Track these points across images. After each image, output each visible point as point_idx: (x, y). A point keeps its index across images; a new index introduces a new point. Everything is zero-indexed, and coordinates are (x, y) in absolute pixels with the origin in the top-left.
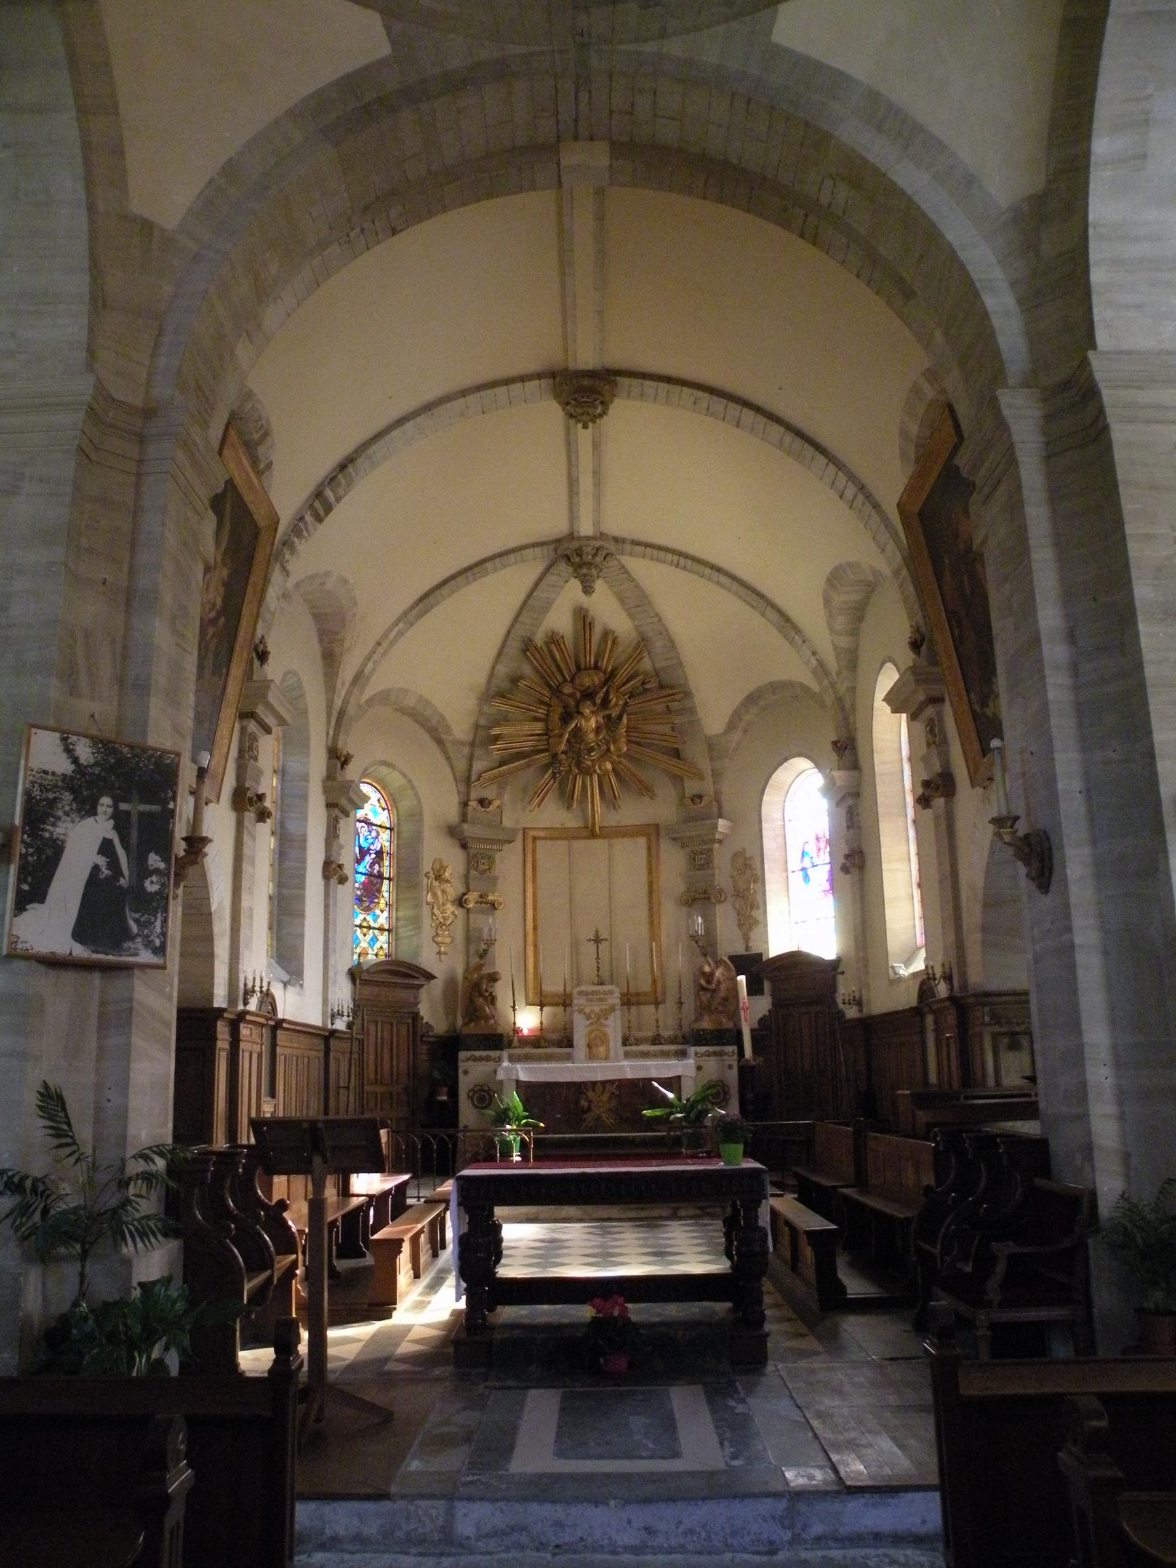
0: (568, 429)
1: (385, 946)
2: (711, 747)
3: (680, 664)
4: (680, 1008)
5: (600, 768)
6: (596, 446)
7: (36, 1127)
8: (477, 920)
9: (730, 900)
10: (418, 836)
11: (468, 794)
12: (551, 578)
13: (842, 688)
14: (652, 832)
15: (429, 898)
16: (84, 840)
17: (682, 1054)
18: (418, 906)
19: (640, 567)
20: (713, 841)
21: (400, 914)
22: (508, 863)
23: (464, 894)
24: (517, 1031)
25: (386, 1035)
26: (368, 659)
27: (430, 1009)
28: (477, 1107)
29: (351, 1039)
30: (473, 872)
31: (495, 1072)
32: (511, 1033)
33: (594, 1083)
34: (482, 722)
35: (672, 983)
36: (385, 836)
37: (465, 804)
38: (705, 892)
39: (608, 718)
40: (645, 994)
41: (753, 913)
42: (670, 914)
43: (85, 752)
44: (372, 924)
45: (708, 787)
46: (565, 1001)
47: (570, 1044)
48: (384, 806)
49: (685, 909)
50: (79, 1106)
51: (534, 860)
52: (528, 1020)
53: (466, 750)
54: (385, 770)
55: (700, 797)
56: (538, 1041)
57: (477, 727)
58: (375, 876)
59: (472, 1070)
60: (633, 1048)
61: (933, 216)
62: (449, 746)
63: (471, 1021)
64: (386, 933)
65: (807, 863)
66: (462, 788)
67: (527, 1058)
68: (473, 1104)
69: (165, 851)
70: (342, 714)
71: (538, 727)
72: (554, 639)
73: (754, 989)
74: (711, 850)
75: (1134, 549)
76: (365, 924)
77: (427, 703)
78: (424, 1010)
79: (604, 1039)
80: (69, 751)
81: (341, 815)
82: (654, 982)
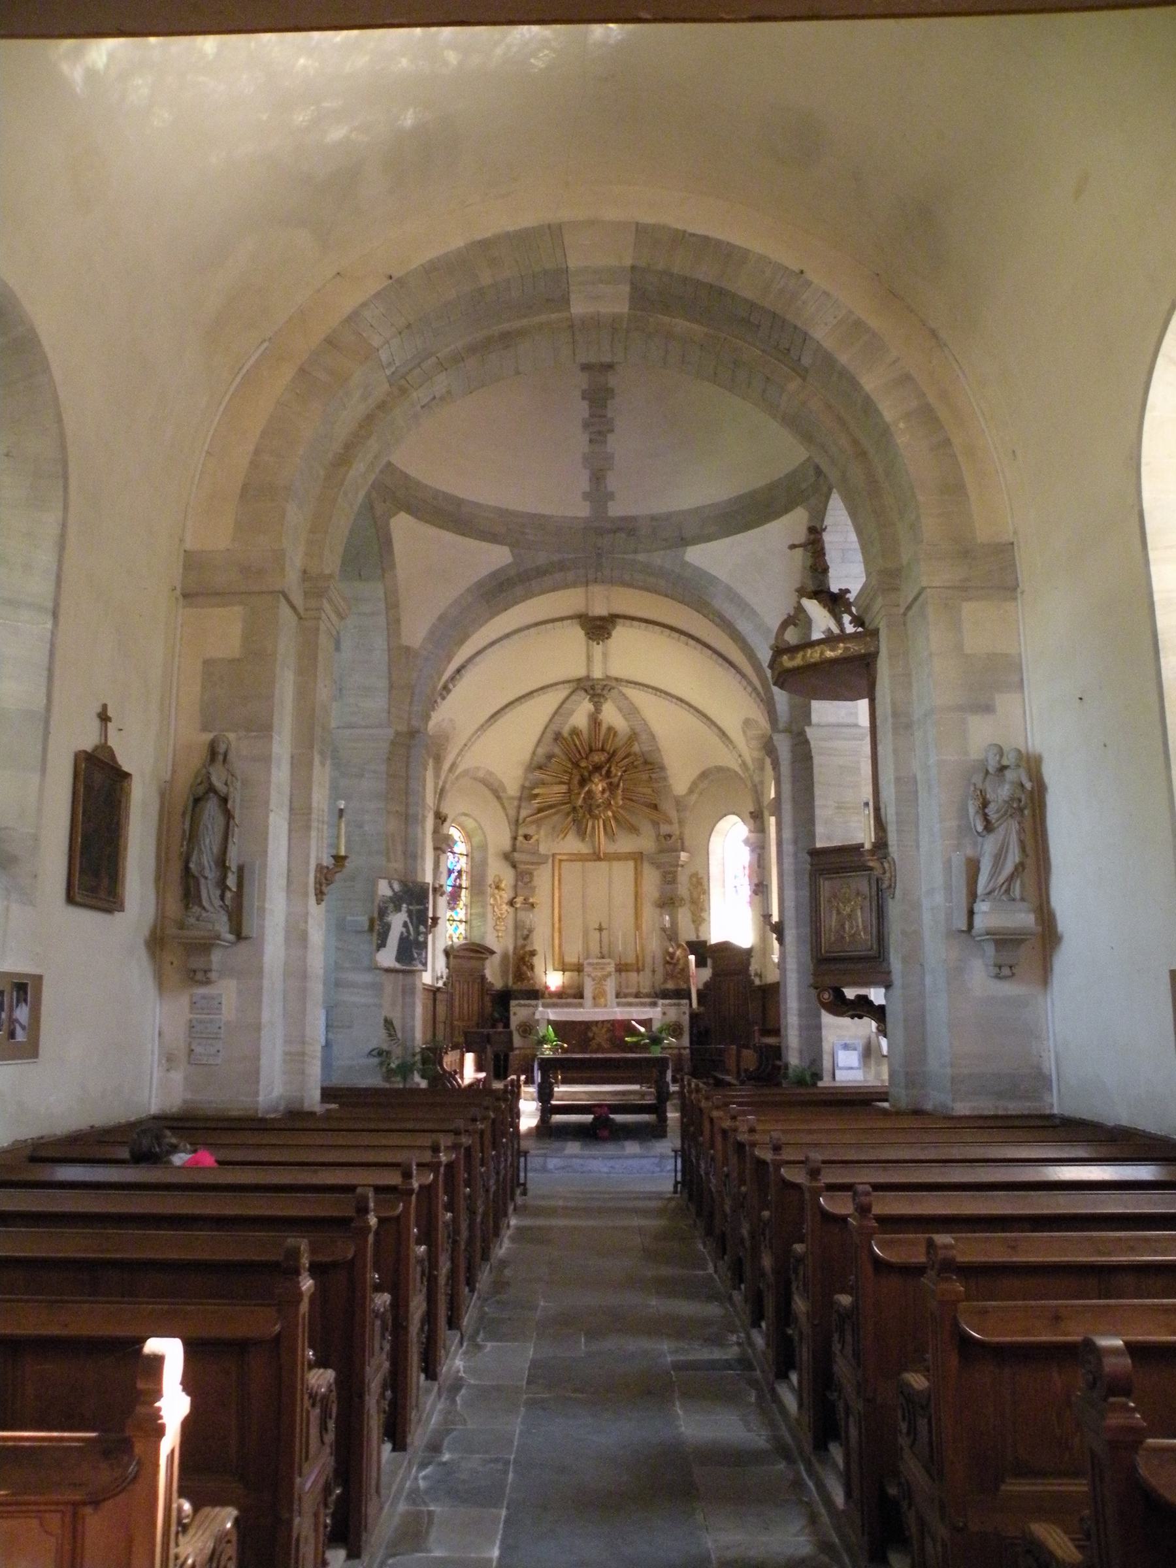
0: (588, 645)
3: (658, 749)
6: (605, 655)
7: (383, 1033)
8: (522, 915)
9: (688, 905)
10: (484, 863)
11: (516, 831)
12: (573, 697)
13: (757, 779)
14: (638, 858)
15: (492, 901)
16: (398, 921)
17: (654, 1004)
19: (630, 692)
22: (543, 878)
24: (547, 988)
26: (458, 755)
27: (492, 973)
33: (597, 1022)
34: (527, 784)
35: (649, 960)
36: (463, 860)
37: (515, 838)
39: (611, 784)
40: (631, 965)
42: (649, 912)
43: (396, 887)
45: (675, 829)
46: (579, 968)
47: (582, 997)
49: (658, 910)
50: (397, 1023)
52: (554, 980)
53: (516, 803)
54: (463, 818)
56: (560, 994)
57: (523, 787)
59: (519, 1012)
60: (623, 1000)
61: (753, 646)
66: (513, 827)
67: (554, 1005)
69: (425, 923)
70: (442, 790)
71: (563, 788)
72: (575, 732)
73: (700, 963)
75: (818, 812)
77: (491, 773)
80: (391, 887)
82: (637, 957)
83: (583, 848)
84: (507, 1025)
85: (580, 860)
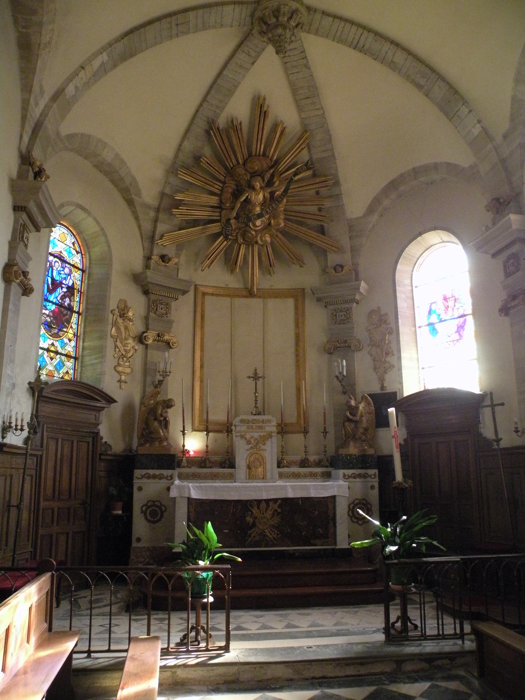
1: (71, 372)
2: (351, 228)
3: (333, 156)
4: (325, 437)
5: (261, 240)
8: (155, 355)
10: (106, 280)
14: (298, 295)
18: (102, 337)
20: (353, 300)
21: (86, 344)
22: (182, 311)
23: (144, 333)
24: (185, 452)
25: (67, 451)
27: (109, 429)
28: (149, 521)
29: (26, 454)
30: (152, 314)
31: (168, 489)
32: (180, 455)
33: (259, 501)
34: (168, 191)
36: (77, 275)
37: (148, 258)
38: (346, 342)
39: (272, 194)
40: (292, 424)
41: (388, 359)
42: (314, 360)
44: (60, 350)
45: (346, 258)
47: (232, 466)
48: (78, 249)
51: (203, 311)
52: (194, 443)
53: (152, 214)
54: (80, 215)
55: (342, 267)
56: (203, 461)
57: (163, 194)
58: (65, 307)
59: (146, 487)
62: (138, 208)
63: (146, 441)
64: (72, 360)
65: (434, 319)
66: (147, 245)
67: (195, 477)
68: (146, 518)
71: (214, 200)
72: (234, 126)
74: (351, 308)
76: (52, 349)
77: (123, 162)
78: (104, 430)
79: (262, 462)
81: (31, 227)
83: (233, 281)
84: (128, 507)
85: (229, 296)
